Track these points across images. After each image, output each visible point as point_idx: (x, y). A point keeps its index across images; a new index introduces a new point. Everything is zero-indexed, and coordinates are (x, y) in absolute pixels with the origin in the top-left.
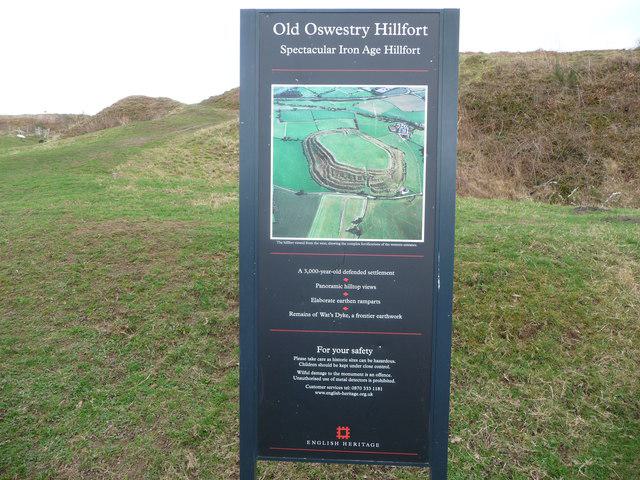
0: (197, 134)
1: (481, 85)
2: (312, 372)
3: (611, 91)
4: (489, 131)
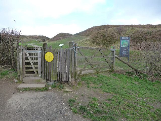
0: (80, 41)
1: (134, 34)
2: (123, 53)
3: (157, 35)
4: (135, 42)
